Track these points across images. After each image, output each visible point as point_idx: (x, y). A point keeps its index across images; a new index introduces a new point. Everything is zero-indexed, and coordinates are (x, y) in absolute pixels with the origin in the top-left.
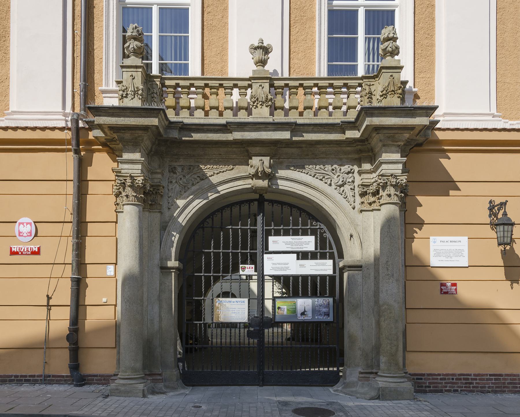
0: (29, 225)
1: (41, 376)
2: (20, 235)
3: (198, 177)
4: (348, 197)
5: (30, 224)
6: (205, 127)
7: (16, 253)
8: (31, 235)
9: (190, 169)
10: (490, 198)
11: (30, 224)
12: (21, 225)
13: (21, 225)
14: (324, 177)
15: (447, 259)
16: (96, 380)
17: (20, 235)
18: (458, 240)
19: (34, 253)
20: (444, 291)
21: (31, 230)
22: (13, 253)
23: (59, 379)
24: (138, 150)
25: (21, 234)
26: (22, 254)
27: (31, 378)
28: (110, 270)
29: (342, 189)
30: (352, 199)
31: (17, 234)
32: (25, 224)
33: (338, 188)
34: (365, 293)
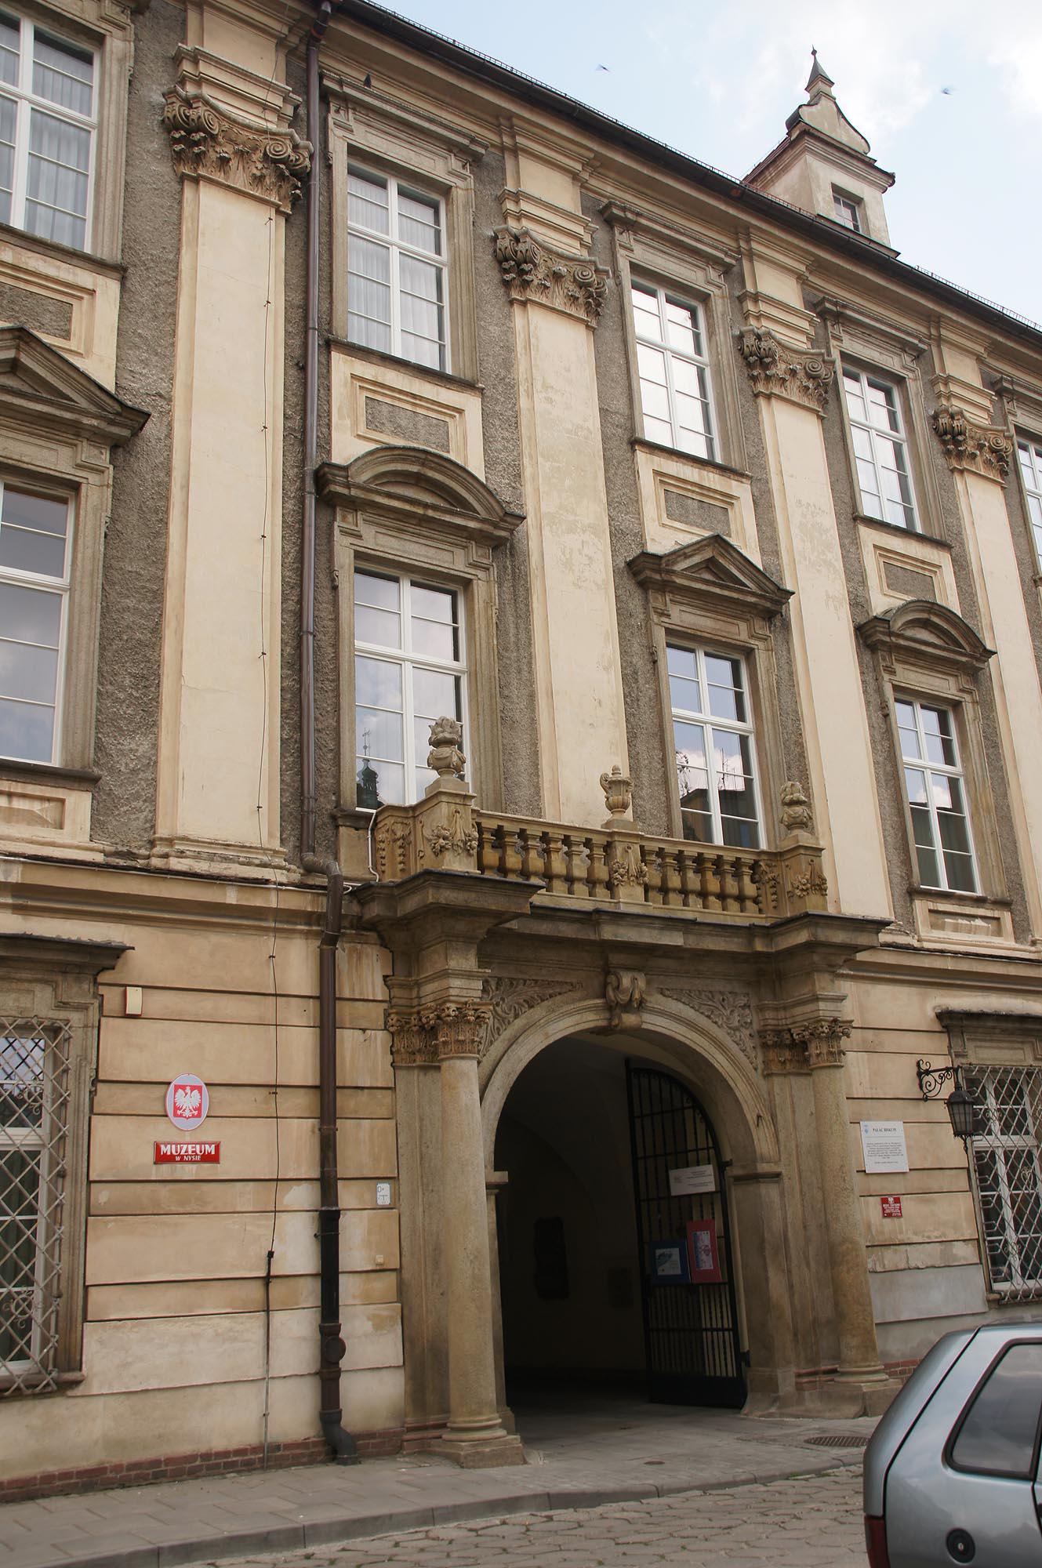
0: (196, 1092)
2: (175, 1115)
5: (200, 1089)
7: (169, 1159)
8: (199, 1116)
10: (918, 1058)
11: (200, 1089)
17: (175, 1115)
22: (161, 1159)
26: (182, 1160)
32: (188, 1090)
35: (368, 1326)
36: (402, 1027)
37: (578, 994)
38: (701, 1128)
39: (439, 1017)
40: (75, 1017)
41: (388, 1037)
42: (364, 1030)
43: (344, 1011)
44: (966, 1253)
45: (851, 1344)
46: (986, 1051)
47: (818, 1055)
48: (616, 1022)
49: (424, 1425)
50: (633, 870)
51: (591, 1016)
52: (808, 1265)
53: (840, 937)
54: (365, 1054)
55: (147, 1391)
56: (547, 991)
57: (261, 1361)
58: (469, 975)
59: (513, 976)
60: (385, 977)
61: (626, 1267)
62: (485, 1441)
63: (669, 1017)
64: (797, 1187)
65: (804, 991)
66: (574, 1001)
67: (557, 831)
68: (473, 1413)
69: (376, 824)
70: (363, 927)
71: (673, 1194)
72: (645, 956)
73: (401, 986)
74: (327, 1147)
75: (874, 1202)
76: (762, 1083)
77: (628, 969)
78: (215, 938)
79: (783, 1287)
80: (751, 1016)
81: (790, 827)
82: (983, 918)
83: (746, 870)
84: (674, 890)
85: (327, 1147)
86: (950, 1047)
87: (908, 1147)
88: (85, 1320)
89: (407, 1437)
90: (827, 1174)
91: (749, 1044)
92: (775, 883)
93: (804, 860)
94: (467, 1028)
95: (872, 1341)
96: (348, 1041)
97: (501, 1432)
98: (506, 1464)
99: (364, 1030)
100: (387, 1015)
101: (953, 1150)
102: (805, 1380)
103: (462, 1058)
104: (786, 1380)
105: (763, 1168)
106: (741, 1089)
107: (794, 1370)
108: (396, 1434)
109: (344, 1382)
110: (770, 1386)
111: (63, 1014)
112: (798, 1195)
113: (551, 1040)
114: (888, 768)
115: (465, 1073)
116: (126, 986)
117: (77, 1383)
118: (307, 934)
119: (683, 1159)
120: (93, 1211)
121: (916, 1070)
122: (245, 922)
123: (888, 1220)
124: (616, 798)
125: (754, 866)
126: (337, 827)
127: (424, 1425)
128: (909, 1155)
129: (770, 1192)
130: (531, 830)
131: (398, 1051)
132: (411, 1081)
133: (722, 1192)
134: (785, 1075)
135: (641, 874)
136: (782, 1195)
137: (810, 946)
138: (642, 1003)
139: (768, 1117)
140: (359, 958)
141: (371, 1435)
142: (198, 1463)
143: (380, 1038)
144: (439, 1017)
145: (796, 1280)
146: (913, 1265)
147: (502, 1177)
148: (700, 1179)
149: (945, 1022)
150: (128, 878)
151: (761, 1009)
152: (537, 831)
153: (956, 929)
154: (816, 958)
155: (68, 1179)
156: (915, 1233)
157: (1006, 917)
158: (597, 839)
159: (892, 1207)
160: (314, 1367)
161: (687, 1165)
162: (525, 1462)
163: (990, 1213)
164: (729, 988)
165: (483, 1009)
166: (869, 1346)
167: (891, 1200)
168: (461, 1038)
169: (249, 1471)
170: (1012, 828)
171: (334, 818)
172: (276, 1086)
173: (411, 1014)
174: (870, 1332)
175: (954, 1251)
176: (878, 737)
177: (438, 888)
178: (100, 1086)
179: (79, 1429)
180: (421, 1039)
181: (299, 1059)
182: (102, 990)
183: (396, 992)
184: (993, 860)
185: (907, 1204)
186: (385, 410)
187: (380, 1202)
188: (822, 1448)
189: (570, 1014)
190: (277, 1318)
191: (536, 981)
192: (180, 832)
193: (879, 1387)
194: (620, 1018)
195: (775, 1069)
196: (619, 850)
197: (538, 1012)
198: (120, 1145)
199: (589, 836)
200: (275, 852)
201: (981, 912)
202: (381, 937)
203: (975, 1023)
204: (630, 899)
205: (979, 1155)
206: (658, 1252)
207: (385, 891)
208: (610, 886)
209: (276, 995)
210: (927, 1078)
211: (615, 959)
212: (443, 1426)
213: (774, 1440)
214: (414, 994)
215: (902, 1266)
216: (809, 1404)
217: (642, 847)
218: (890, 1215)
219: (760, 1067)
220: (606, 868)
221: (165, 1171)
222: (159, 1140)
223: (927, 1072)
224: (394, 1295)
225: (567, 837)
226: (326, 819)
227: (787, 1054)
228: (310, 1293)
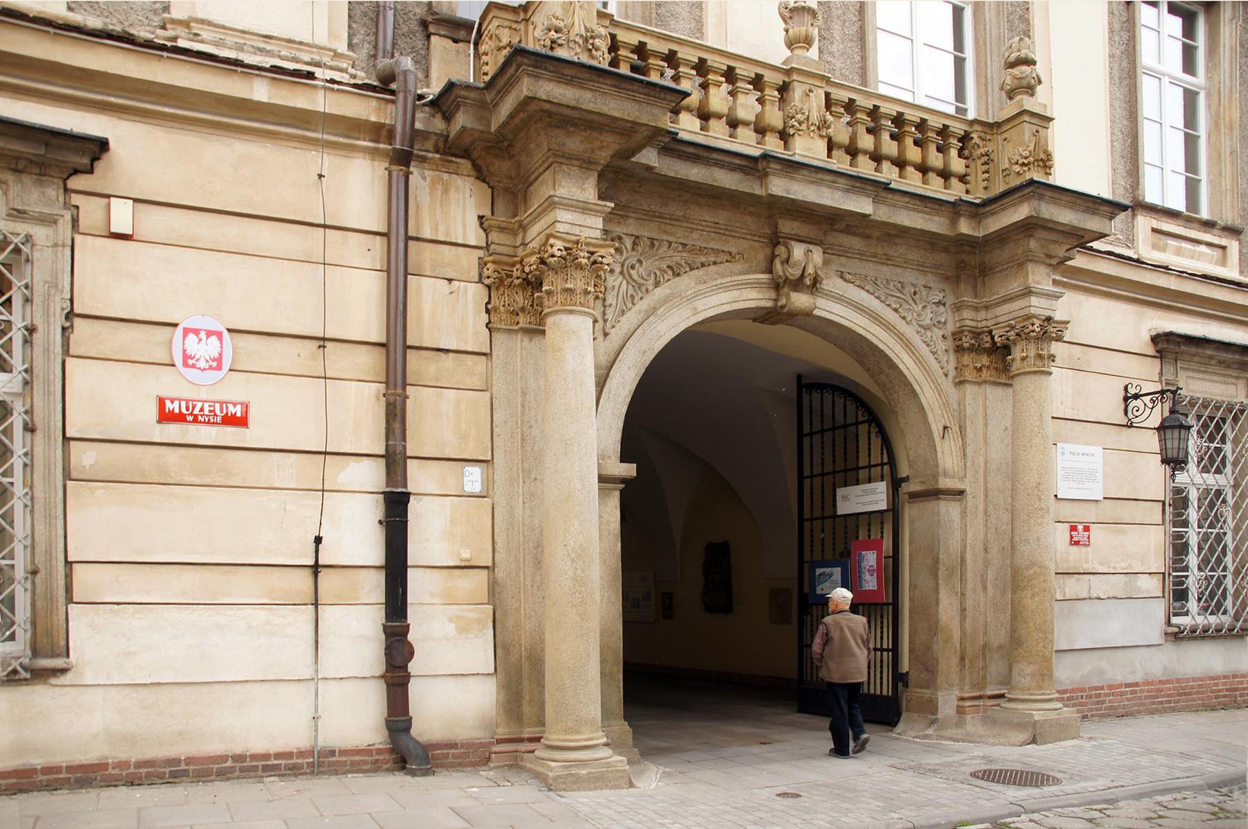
0: (214, 339)
1: (310, 753)
2: (185, 365)
3: (669, 267)
5: (219, 335)
6: (715, 156)
7: (179, 418)
8: (219, 368)
9: (652, 245)
10: (1127, 381)
11: (219, 335)
12: (191, 336)
13: (191, 336)
16: (454, 756)
17: (185, 365)
19: (229, 420)
21: (220, 355)
23: (357, 758)
25: (190, 362)
26: (195, 420)
27: (282, 762)
28: (471, 478)
31: (179, 361)
32: (203, 335)
35: (450, 629)
36: (501, 280)
37: (738, 267)
38: (876, 442)
39: (543, 262)
40: (40, 233)
41: (485, 292)
42: (450, 280)
43: (422, 255)
44: (1152, 586)
45: (1025, 672)
46: (1198, 382)
47: (1023, 359)
48: (783, 302)
49: (518, 735)
50: (815, 117)
51: (753, 294)
52: (985, 588)
53: (1066, 216)
54: (450, 308)
55: (159, 684)
56: (697, 259)
57: (310, 658)
58: (584, 208)
59: (654, 235)
60: (481, 218)
61: (757, 551)
62: (583, 763)
63: (848, 303)
64: (981, 507)
65: (1015, 286)
66: (732, 274)
67: (718, 58)
68: (568, 731)
69: (480, 34)
70: (454, 151)
71: (839, 513)
72: (824, 224)
73: (502, 229)
74: (395, 415)
77: (801, 241)
78: (239, 148)
79: (955, 611)
80: (945, 315)
81: (1011, 95)
82: (1209, 244)
83: (954, 141)
84: (865, 152)
85: (395, 415)
86: (1161, 374)
87: (1105, 475)
88: (69, 599)
89: (496, 748)
90: (1019, 492)
91: (941, 346)
92: (988, 160)
93: (1028, 129)
94: (578, 274)
95: (1050, 669)
96: (427, 296)
97: (607, 752)
98: (607, 787)
99: (450, 280)
100: (482, 264)
101: (1152, 478)
102: (968, 703)
103: (571, 312)
104: (947, 703)
105: (945, 483)
106: (928, 396)
107: (957, 693)
108: (482, 745)
109: (414, 688)
110: (929, 708)
111: (22, 228)
112: (981, 515)
113: (700, 318)
114: (1124, 64)
115: (574, 338)
116: (108, 196)
117: (64, 671)
118: (373, 153)
119: (852, 475)
120: (74, 474)
121: (1122, 394)
122: (283, 129)
123: (1075, 548)
124: (798, 29)
125: (965, 139)
126: (428, 37)
127: (518, 735)
129: (949, 510)
130: (684, 53)
131: (495, 309)
132: (511, 348)
133: (894, 510)
134: (979, 384)
135: (824, 124)
136: (964, 513)
137: (1029, 226)
138: (816, 280)
140: (446, 191)
141: (452, 745)
142: (229, 764)
143: (473, 294)
144: (543, 262)
145: (969, 603)
147: (630, 470)
148: (869, 497)
149: (1160, 346)
150: (103, 50)
151: (958, 308)
152: (692, 56)
153: (1178, 252)
154: (1033, 244)
155: (39, 435)
156: (1102, 564)
157: (1233, 246)
158: (770, 77)
159: (1080, 535)
160: (380, 668)
161: (857, 483)
162: (631, 785)
163: (1180, 548)
164: (922, 280)
165: (602, 252)
166: (1045, 674)
167: (1080, 527)
168: (568, 286)
169: (296, 775)
171: (424, 24)
172: (324, 339)
173: (513, 265)
174: (1048, 660)
175: (1139, 583)
176: (1117, 26)
177: (537, 77)
178: (78, 322)
179: (65, 722)
180: (521, 291)
181: (359, 307)
182: (76, 199)
183: (494, 236)
184: (1227, 183)
186: (654, 22)
187: (468, 488)
188: (999, 787)
189: (725, 288)
190: (327, 613)
191: (684, 245)
192: (200, 15)
193: (1052, 716)
194: (788, 297)
196: (797, 92)
197: (686, 282)
198: (108, 395)
199: (760, 71)
200: (337, 55)
201: (1207, 237)
202: (476, 167)
203: (1193, 350)
204: (809, 149)
205: (1178, 491)
206: (819, 571)
207: (473, 95)
208: (784, 136)
209: (325, 226)
210: (1134, 403)
211: (787, 226)
212: (538, 740)
213: (934, 771)
214: (519, 242)
216: (970, 728)
217: (827, 95)
218: (1077, 543)
219: (952, 373)
220: (781, 113)
221: (173, 432)
222: (163, 395)
223: (1136, 396)
224: (484, 596)
225: (731, 70)
226: (414, 26)
227: (985, 360)
228: (374, 587)
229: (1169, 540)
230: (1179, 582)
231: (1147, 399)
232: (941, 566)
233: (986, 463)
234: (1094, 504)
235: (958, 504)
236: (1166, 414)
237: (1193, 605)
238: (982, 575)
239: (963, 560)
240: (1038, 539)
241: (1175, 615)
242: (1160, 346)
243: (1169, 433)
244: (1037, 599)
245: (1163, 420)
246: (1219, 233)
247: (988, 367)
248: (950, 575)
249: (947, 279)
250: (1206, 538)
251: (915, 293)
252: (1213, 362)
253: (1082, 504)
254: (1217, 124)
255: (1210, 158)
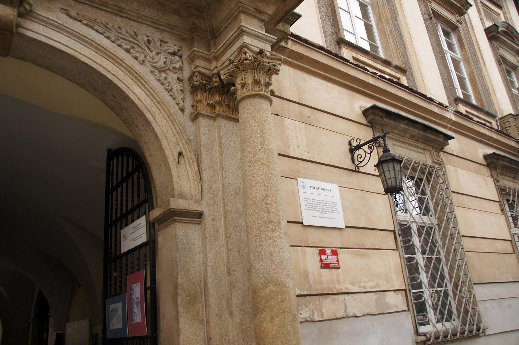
4: (174, 90)
14: (133, 48)
15: (322, 215)
18: (329, 188)
20: (325, 262)
24: (285, 185)
29: (163, 75)
30: (181, 96)
33: (157, 72)
34: (212, 267)
44: (397, 301)
46: (401, 149)
52: (231, 314)
64: (222, 230)
75: (312, 255)
76: (189, 124)
87: (344, 207)
90: (252, 216)
91: (176, 87)
112: (222, 238)
121: (348, 147)
123: (326, 271)
128: (345, 215)
129: (181, 232)
134: (214, 118)
136: (204, 235)
139: (188, 154)
146: (351, 314)
149: (370, 118)
151: (192, 59)
156: (353, 284)
159: (329, 258)
163: (412, 269)
167: (329, 251)
170: (401, 36)
175: (388, 300)
185: (344, 256)
195: (201, 109)
215: (341, 314)
218: (327, 266)
219: (188, 110)
223: (358, 147)
229: (404, 262)
230: (418, 297)
231: (365, 148)
232: (180, 292)
233: (223, 186)
234: (337, 232)
235: (197, 227)
236: (381, 153)
237: (431, 314)
238: (227, 300)
239: (206, 285)
240: (271, 253)
241: (421, 324)
242: (370, 118)
243: (385, 167)
244: (276, 322)
245: (380, 159)
246: (394, 69)
247: (220, 103)
248: (193, 299)
249: (184, 40)
250: (429, 260)
251: (149, 42)
252: (407, 135)
253: (329, 231)
254: (380, 19)
255: (380, 35)
